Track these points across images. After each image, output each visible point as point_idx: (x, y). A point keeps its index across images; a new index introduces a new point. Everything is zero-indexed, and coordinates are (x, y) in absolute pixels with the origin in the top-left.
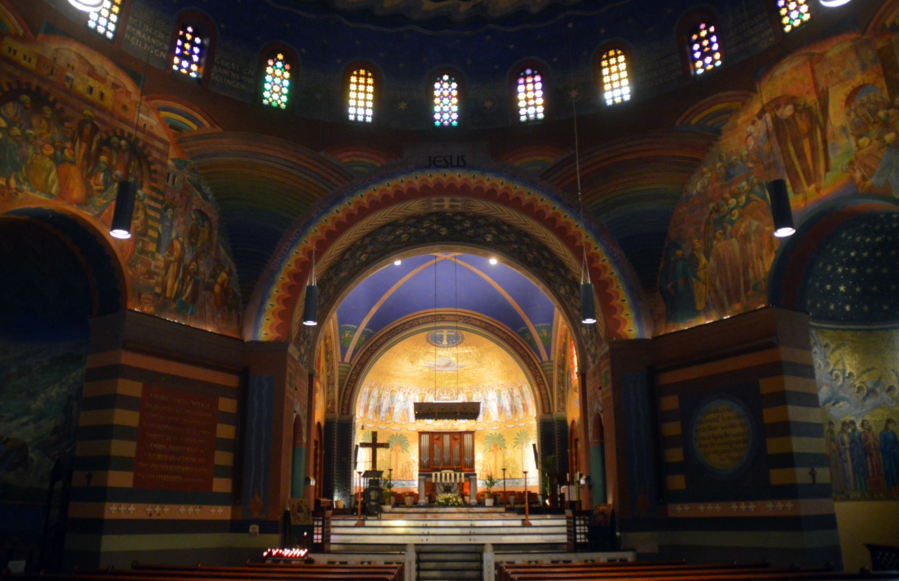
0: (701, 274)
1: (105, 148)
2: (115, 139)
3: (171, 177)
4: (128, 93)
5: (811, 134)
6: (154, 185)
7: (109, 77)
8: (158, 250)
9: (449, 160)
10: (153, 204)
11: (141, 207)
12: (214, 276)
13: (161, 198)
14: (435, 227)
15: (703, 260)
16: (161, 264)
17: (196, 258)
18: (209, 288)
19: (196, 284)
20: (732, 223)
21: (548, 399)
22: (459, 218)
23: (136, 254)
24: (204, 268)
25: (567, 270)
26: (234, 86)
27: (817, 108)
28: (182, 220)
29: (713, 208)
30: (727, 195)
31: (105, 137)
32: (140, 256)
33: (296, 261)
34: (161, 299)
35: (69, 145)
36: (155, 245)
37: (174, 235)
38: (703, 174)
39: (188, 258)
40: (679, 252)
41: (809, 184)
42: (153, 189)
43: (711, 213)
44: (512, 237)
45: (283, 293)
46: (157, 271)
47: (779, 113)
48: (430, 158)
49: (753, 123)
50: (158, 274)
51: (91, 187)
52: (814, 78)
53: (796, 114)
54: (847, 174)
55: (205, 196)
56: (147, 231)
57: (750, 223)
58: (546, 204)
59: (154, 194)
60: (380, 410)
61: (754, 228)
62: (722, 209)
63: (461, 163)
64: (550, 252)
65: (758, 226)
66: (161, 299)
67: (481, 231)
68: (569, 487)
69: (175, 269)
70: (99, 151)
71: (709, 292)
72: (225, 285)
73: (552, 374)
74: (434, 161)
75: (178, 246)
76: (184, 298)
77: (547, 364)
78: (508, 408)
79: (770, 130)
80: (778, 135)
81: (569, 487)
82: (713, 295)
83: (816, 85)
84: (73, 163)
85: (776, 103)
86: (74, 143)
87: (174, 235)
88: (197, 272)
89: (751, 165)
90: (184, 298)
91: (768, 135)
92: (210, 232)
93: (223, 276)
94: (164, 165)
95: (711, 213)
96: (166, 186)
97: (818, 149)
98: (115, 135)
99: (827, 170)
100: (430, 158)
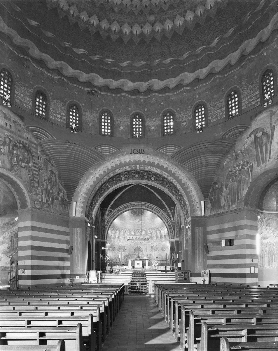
0: (224, 194)
1: (15, 148)
2: (18, 144)
3: (40, 158)
4: (20, 125)
5: (266, 145)
6: (34, 161)
7: (12, 118)
8: (38, 186)
9: (138, 151)
10: (35, 169)
11: (31, 170)
12: (58, 194)
13: (37, 166)
14: (134, 175)
15: (225, 189)
16: (40, 191)
17: (52, 188)
18: (57, 198)
19: (53, 197)
20: (236, 176)
21: (173, 234)
22: (142, 171)
23: (31, 187)
24: (55, 192)
25: (179, 191)
26: (59, 120)
27: (270, 134)
28: (45, 174)
29: (230, 170)
30: (235, 166)
31: (14, 144)
32: (33, 188)
33: (86, 189)
34: (42, 203)
35: (2, 147)
36: (37, 184)
37: (43, 180)
38: (228, 157)
39: (49, 188)
40: (217, 186)
41: (263, 164)
42: (34, 163)
43: (229, 172)
44: (161, 179)
45: (82, 200)
46: (39, 193)
47: (257, 135)
48: (132, 149)
49: (248, 138)
50: (39, 194)
51: (13, 163)
52: (271, 121)
53: (263, 135)
54: (276, 160)
55: (52, 165)
56: (34, 179)
57: (241, 176)
58: (172, 167)
59: (35, 165)
60: (115, 237)
61: (242, 178)
62: (233, 171)
63: (143, 152)
64: (173, 184)
65: (244, 178)
66: (42, 203)
67: (150, 176)
68: (83, 326)
69: (45, 193)
70: (13, 149)
71: (225, 200)
72: (62, 197)
73: (175, 225)
74: (133, 151)
75: (45, 184)
76: (49, 203)
77: (173, 222)
78: (159, 237)
79: (253, 141)
80: (255, 144)
81: (83, 326)
82: (227, 201)
83: (271, 124)
84: (4, 154)
85: (256, 131)
86: (4, 146)
87: (43, 180)
88: (53, 193)
89: (245, 155)
90: (49, 203)
91: (252, 143)
92: (56, 178)
93: (61, 194)
94: (36, 153)
95: (229, 172)
96: (38, 162)
97: (268, 150)
98: (18, 142)
99: (270, 158)
100: (132, 149)
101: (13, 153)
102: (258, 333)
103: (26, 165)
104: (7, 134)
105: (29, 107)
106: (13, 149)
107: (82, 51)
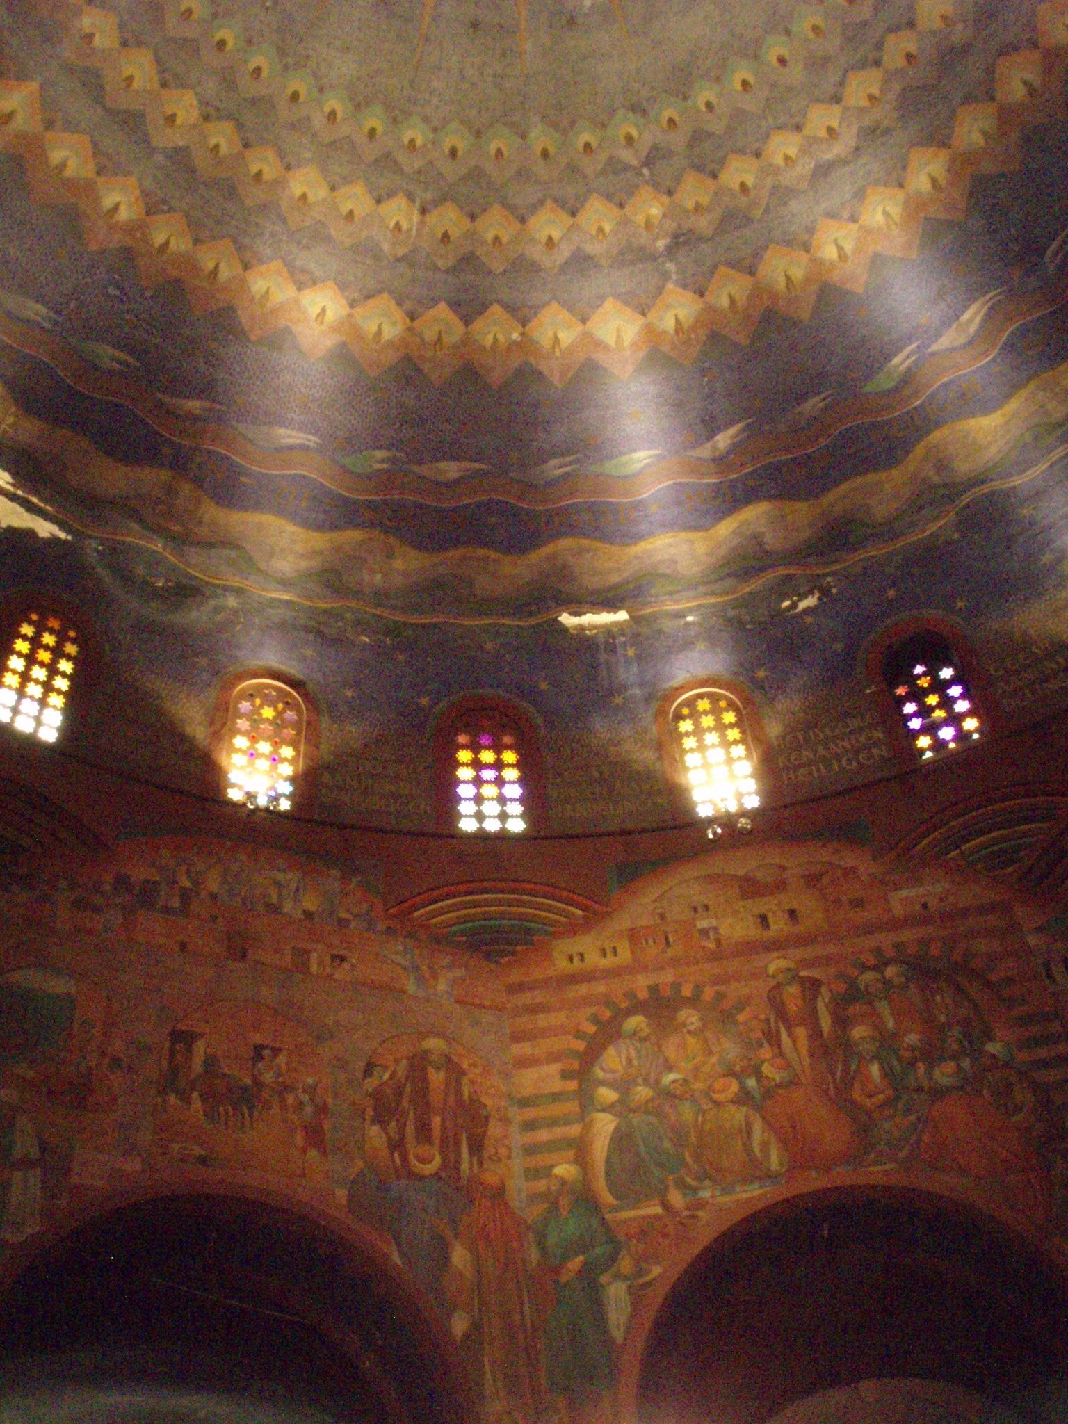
4: (850, 872)
101: (848, 1047)
102: (32, 1181)
103: (966, 1063)
104: (783, 963)
105: (871, 757)
106: (842, 1023)
107: (971, 320)
